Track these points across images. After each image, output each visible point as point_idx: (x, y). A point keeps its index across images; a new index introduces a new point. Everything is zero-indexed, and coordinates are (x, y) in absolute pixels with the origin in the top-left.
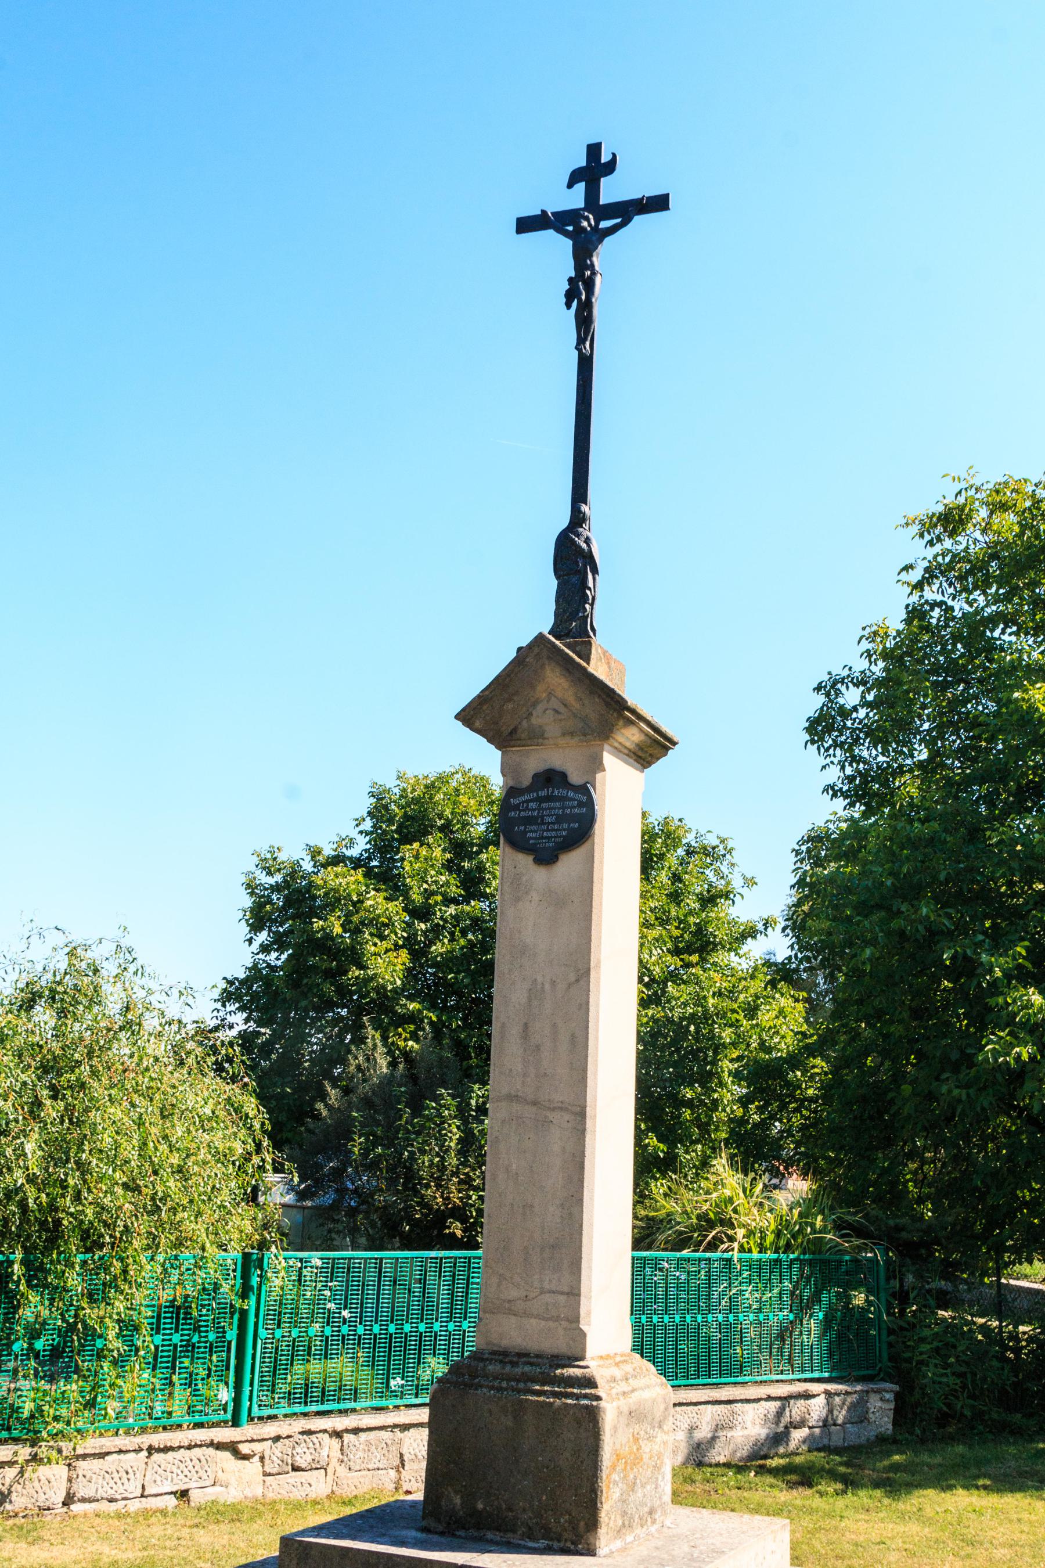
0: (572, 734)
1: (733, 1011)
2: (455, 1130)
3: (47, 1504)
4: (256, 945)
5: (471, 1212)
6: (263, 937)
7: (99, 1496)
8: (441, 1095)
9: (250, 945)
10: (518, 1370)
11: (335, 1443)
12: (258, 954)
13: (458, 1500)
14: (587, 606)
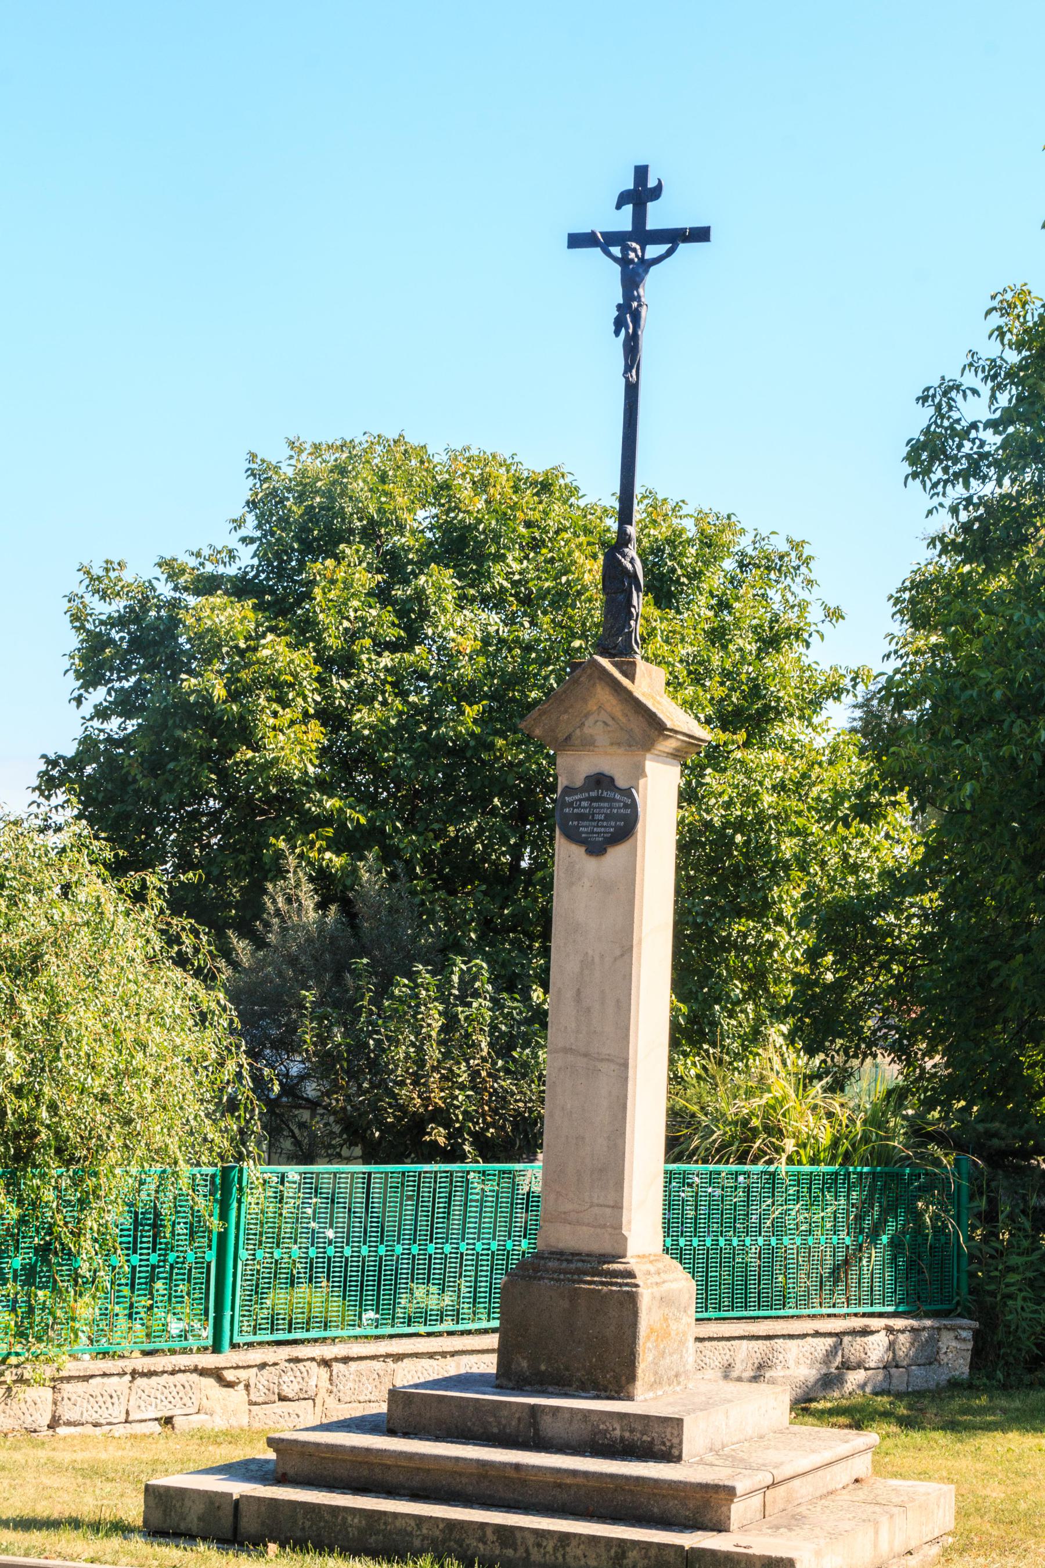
0: (619, 744)
1: (799, 814)
2: (437, 1016)
3: (34, 1426)
4: (87, 709)
5: (457, 1116)
6: (99, 695)
7: (84, 1420)
8: (419, 972)
9: (78, 707)
10: (573, 1266)
11: (323, 1371)
12: (91, 719)
13: (525, 1364)
14: (632, 623)
